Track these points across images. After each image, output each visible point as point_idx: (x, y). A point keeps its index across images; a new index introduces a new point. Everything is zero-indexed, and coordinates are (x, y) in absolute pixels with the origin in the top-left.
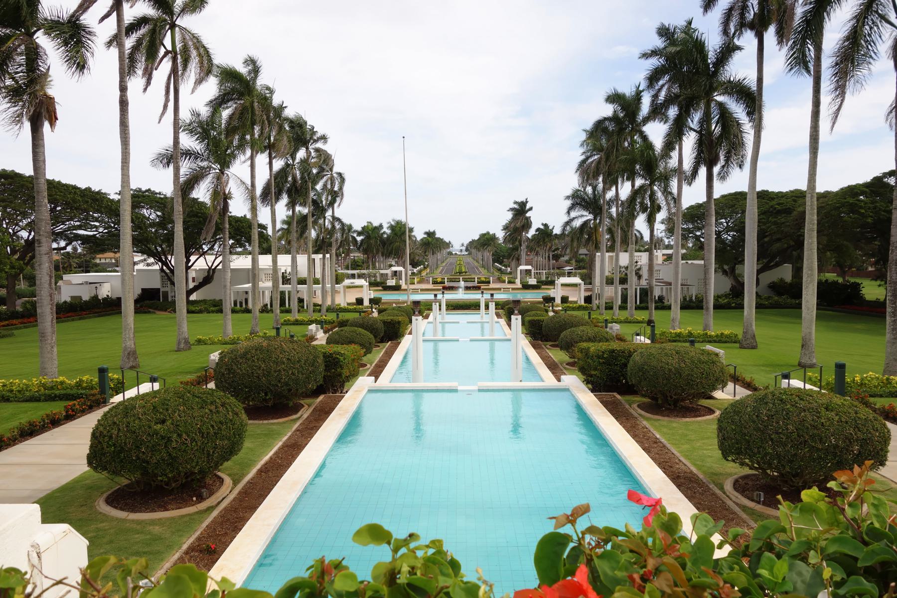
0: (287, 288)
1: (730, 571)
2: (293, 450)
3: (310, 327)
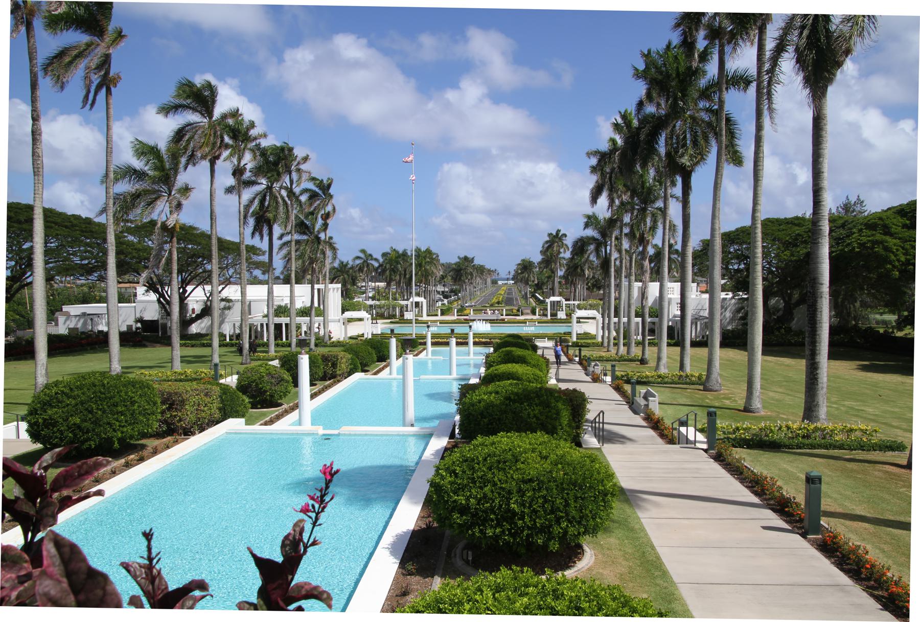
0: (283, 320)
1: (642, 395)
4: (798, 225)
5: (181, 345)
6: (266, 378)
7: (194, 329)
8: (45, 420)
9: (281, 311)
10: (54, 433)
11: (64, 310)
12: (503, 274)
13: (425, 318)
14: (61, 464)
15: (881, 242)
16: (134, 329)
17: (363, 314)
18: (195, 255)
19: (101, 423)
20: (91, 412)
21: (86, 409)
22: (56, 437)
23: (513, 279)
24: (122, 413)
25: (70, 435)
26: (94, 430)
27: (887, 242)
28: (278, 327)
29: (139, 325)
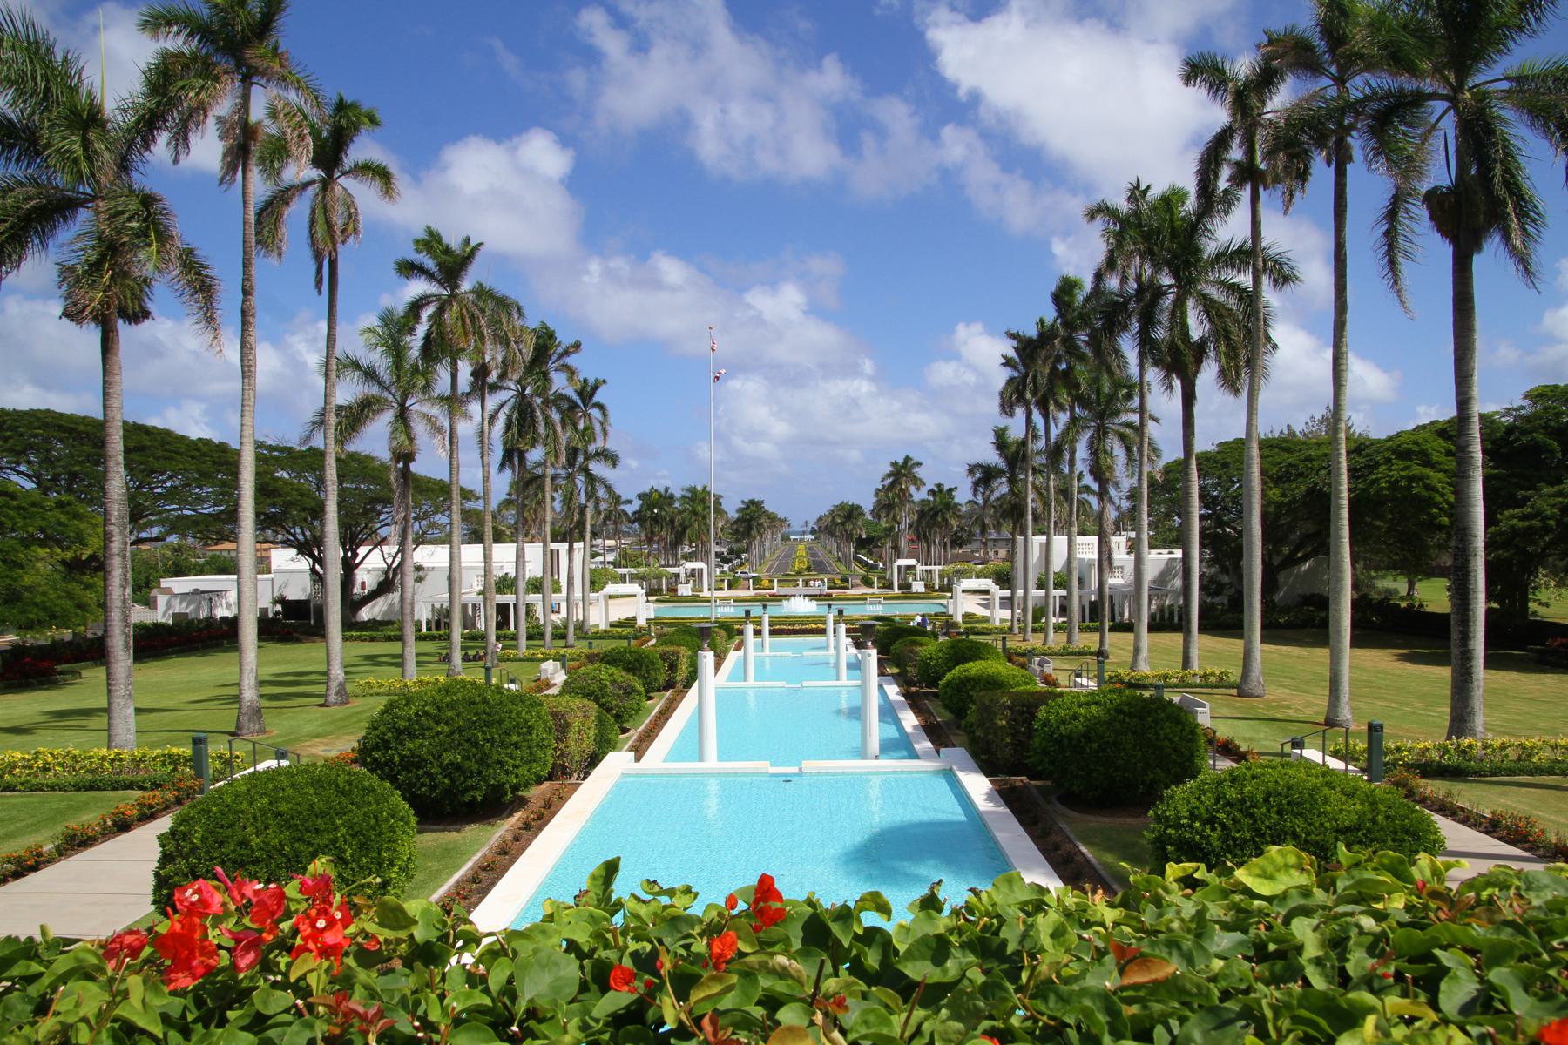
0: (508, 598)
2: (506, 855)
3: (544, 665)
4: (1288, 450)
5: (345, 639)
6: (610, 688)
7: (365, 614)
8: (402, 757)
9: (505, 584)
10: (418, 778)
11: (163, 585)
12: (797, 525)
13: (706, 593)
14: (427, 827)
15: (1421, 478)
16: (271, 615)
17: (634, 588)
18: (374, 501)
19: (490, 761)
20: (476, 745)
21: (468, 740)
22: (423, 785)
23: (813, 532)
24: (516, 746)
25: (446, 781)
26: (479, 773)
27: (1428, 478)
28: (503, 610)
29: (279, 608)
